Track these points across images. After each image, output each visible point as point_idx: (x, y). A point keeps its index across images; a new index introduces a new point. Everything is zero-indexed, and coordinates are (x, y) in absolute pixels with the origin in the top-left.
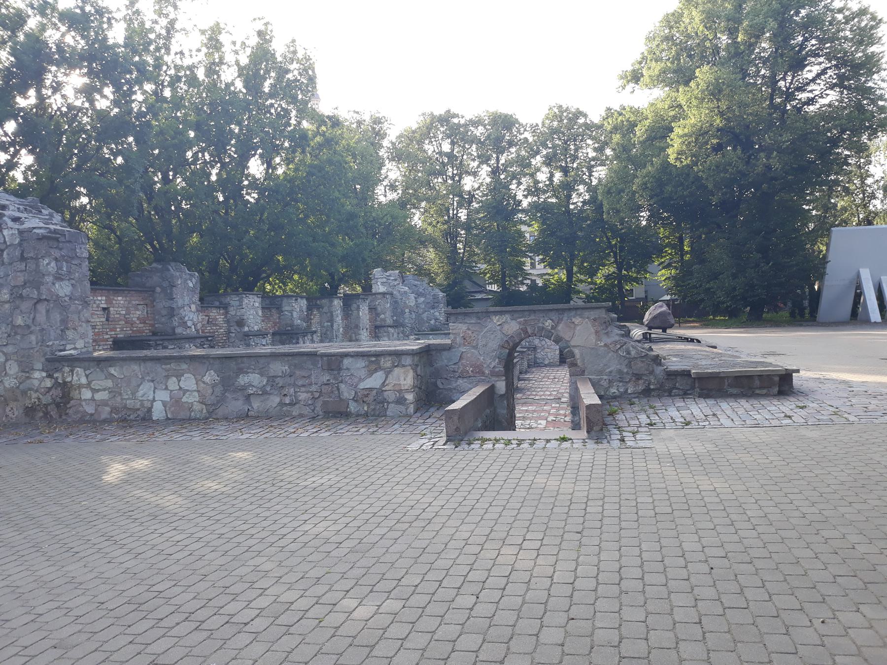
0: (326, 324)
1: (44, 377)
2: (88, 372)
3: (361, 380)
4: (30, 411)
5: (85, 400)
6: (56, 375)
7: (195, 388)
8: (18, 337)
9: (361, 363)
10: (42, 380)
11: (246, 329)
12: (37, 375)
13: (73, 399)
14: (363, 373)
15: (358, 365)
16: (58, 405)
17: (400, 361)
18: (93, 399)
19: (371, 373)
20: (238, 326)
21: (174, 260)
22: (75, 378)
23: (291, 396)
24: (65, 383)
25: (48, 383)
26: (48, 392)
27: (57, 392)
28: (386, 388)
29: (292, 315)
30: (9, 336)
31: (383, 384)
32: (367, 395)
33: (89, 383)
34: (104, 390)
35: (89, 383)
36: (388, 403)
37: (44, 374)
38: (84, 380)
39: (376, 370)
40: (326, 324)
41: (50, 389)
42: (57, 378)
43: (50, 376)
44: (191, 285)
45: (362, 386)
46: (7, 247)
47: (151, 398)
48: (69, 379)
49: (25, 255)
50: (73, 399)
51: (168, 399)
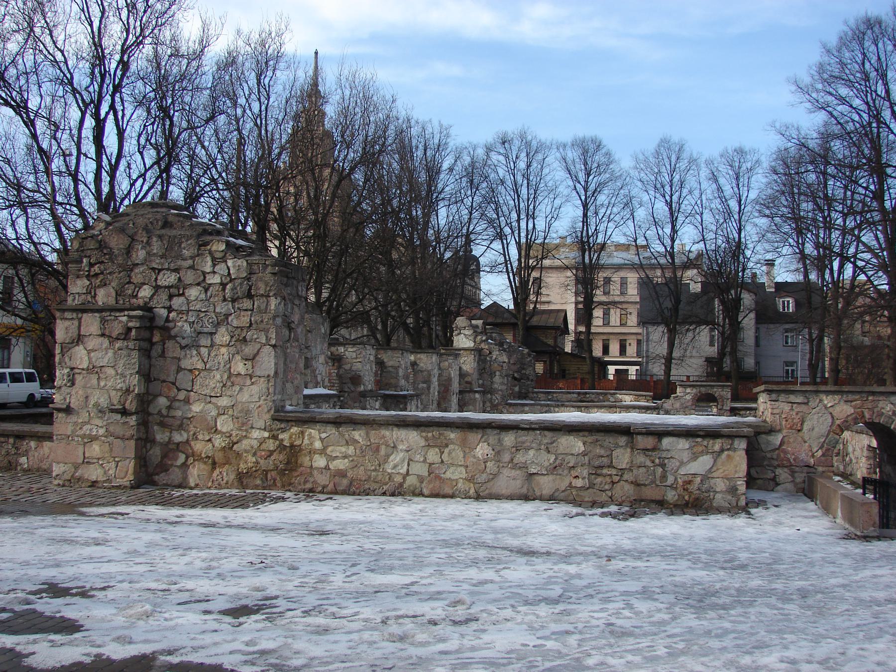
0: (421, 386)
1: (265, 439)
2: (324, 435)
3: (682, 463)
4: (242, 479)
5: (316, 468)
6: (281, 437)
7: (462, 463)
8: (237, 388)
9: (683, 444)
10: (262, 441)
11: (362, 388)
12: (256, 434)
13: (301, 466)
14: (685, 456)
15: (680, 446)
16: (282, 473)
17: (732, 444)
18: (327, 468)
19: (695, 457)
20: (353, 383)
21: (670, 331)
22: (306, 441)
23: (584, 478)
24: (292, 446)
25: (271, 445)
26: (269, 456)
27: (279, 458)
28: (715, 475)
29: (398, 373)
30: (224, 385)
31: (710, 471)
32: (690, 482)
33: (325, 448)
34: (345, 457)
35: (325, 448)
36: (716, 492)
37: (266, 434)
38: (318, 445)
39: (702, 453)
40: (421, 386)
41: (271, 453)
42: (282, 440)
43: (275, 437)
44: (323, 331)
45: (682, 471)
46: (231, 280)
47: (403, 471)
48: (297, 443)
49: (253, 292)
50: (301, 466)
51: (426, 474)
